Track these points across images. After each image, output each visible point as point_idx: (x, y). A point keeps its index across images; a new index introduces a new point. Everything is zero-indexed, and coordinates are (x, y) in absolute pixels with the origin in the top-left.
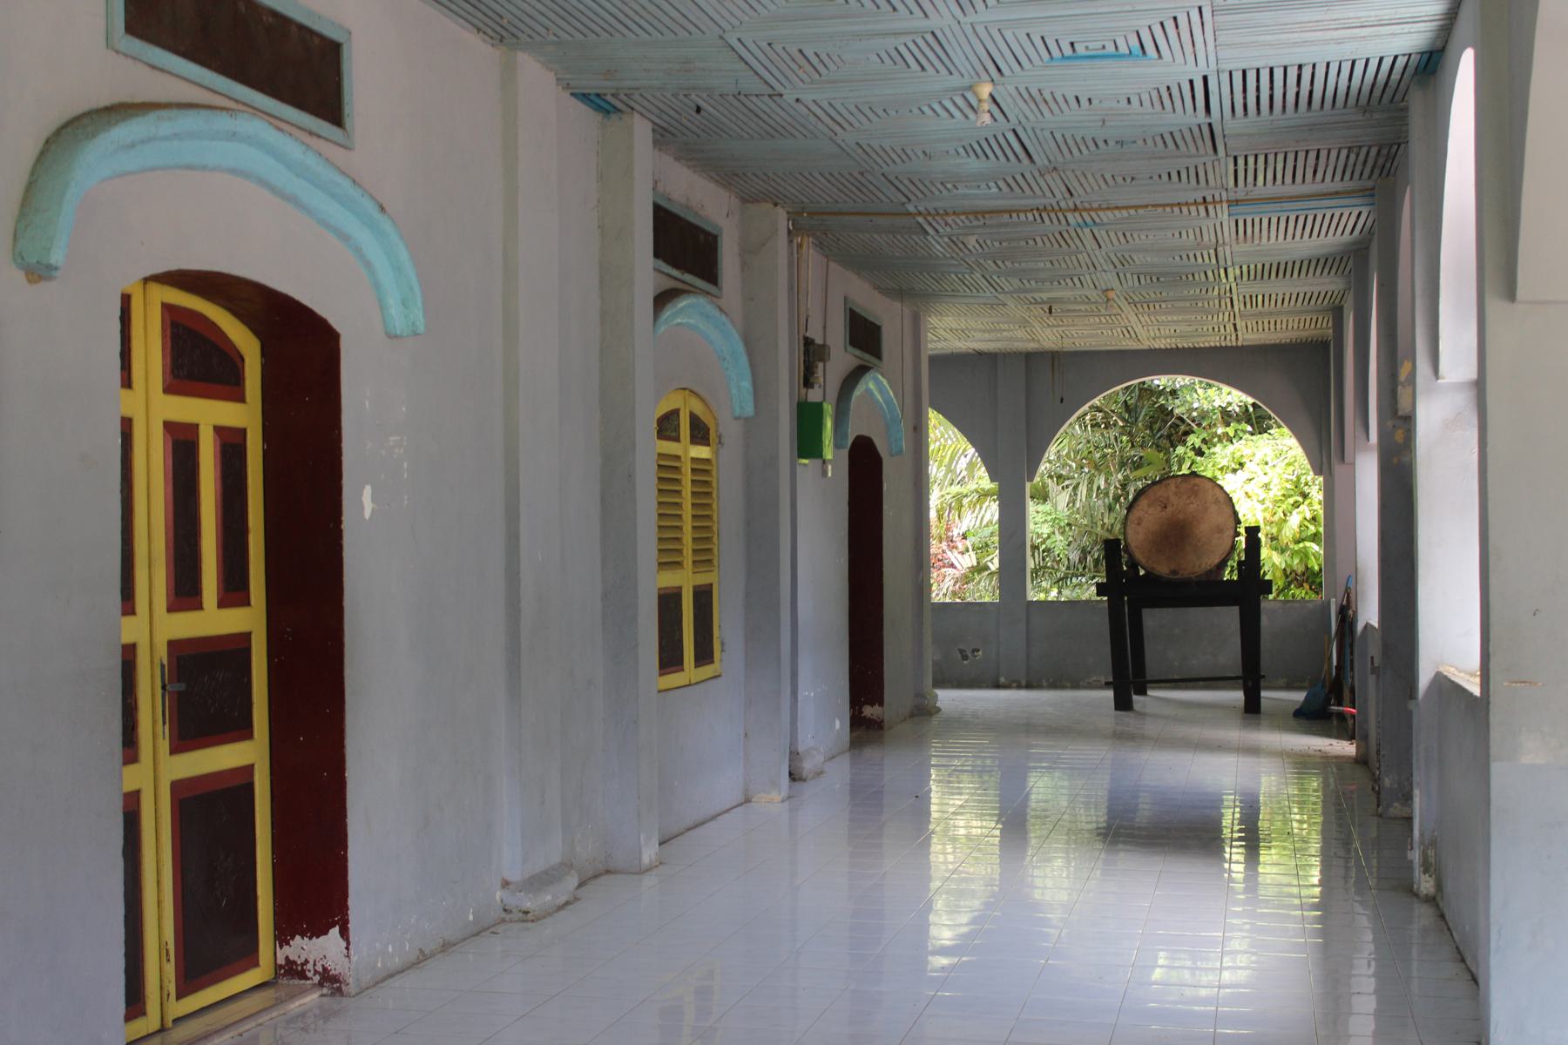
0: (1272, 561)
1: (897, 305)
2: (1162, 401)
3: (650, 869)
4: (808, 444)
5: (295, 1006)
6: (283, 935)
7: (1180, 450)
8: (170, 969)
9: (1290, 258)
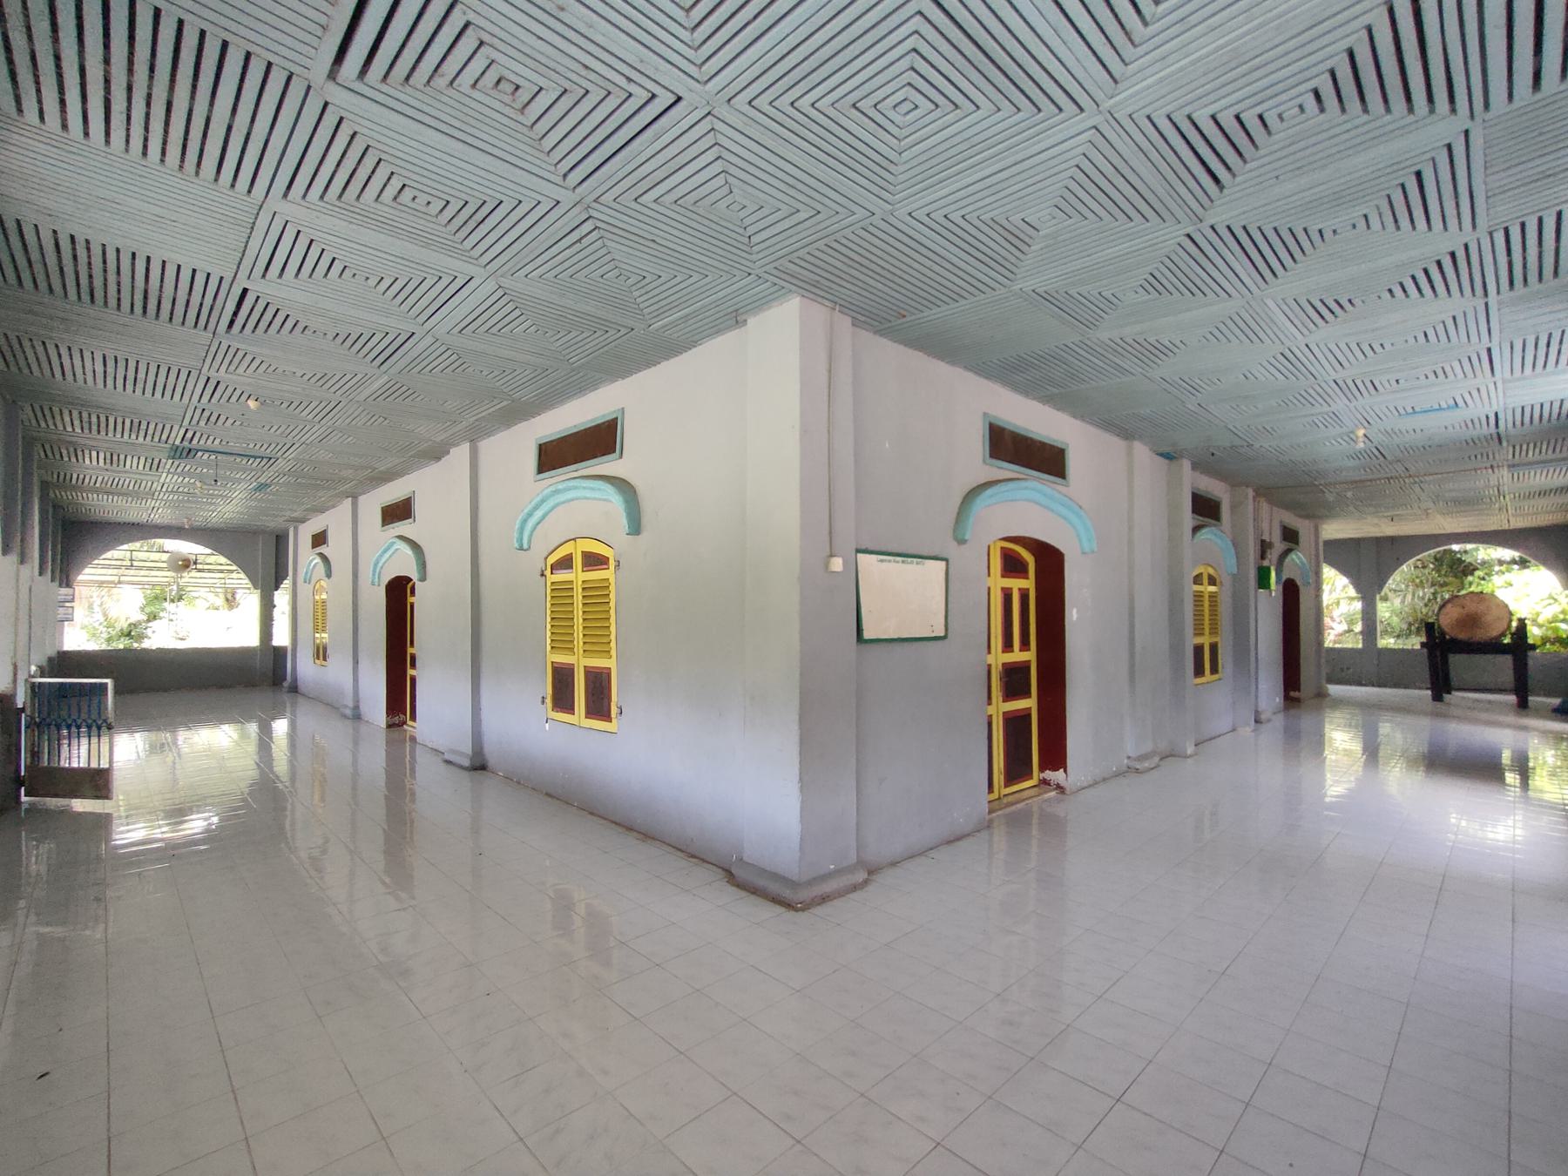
0: (1534, 633)
1: (1307, 521)
2: (1459, 556)
3: (1190, 756)
4: (1263, 581)
5: (1047, 796)
6: (1042, 769)
7: (1470, 578)
8: (1002, 777)
9: (1552, 487)
